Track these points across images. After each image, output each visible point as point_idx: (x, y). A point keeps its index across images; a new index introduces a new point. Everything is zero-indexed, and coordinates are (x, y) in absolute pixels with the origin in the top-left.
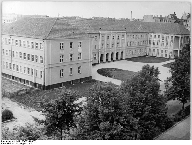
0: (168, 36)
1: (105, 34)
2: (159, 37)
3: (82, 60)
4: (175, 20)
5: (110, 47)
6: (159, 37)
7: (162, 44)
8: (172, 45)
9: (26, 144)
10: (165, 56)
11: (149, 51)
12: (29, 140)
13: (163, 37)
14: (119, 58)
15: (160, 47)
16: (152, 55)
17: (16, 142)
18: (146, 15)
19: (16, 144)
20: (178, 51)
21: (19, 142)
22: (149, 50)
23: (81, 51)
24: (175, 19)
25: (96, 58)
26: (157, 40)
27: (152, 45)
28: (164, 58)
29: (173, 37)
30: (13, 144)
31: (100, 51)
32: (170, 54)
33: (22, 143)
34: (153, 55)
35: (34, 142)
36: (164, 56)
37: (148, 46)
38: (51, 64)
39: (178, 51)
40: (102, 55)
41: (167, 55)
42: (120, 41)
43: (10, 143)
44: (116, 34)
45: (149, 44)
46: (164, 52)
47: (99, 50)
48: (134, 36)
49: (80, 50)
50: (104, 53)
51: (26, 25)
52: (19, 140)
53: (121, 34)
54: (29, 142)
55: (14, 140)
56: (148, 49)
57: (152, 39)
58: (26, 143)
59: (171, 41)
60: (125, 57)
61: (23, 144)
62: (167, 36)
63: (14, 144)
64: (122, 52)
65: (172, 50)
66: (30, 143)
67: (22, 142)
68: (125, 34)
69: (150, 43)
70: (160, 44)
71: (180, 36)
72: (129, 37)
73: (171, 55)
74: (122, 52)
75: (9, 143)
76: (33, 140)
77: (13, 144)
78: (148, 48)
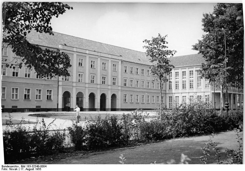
0: (185, 72)
2: (184, 73)
6: (184, 73)
7: (191, 86)
9: (33, 170)
11: (170, 101)
12: (37, 165)
15: (195, 90)
17: (21, 168)
19: (20, 169)
21: (24, 168)
22: (170, 99)
25: (52, 98)
27: (174, 90)
31: (60, 83)
33: (28, 168)
35: (44, 167)
37: (167, 92)
43: (13, 168)
44: (99, 59)
45: (169, 89)
47: (58, 81)
48: (139, 70)
50: (85, 92)
52: (24, 165)
54: (37, 167)
55: (18, 165)
56: (168, 98)
58: (33, 168)
60: (120, 106)
61: (30, 169)
63: (18, 169)
64: (114, 96)
67: (28, 167)
68: (118, 62)
70: (188, 85)
75: (12, 168)
76: (42, 165)
78: (168, 96)
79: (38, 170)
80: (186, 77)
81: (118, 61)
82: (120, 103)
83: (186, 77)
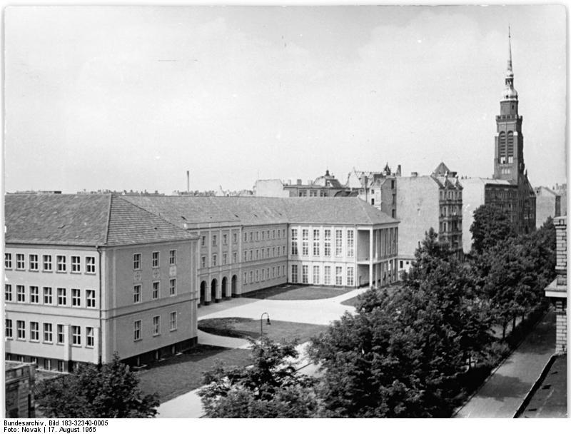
0: (341, 231)
1: (197, 231)
2: (327, 233)
3: (179, 296)
4: (335, 191)
5: (208, 265)
7: (327, 252)
8: (352, 252)
9: (77, 433)
10: (337, 280)
11: (293, 272)
12: (85, 420)
13: (327, 233)
14: (229, 294)
15: (332, 259)
16: (302, 282)
18: (260, 181)
20: (368, 266)
22: (293, 269)
23: (175, 273)
24: (338, 188)
26: (310, 241)
28: (335, 286)
29: (352, 231)
30: (37, 430)
32: (348, 275)
33: (65, 427)
34: (304, 282)
36: (333, 282)
37: (290, 258)
38: (117, 309)
39: (368, 266)
40: (203, 285)
41: (341, 277)
42: (208, 251)
43: (30, 427)
45: (293, 253)
46: (333, 270)
49: (173, 271)
51: (22, 215)
53: (230, 229)
54: (86, 426)
55: (41, 420)
56: (291, 267)
57: (299, 241)
58: (77, 427)
59: (350, 242)
60: (302, 280)
62: (337, 231)
63: (42, 430)
64: (234, 278)
65: (355, 266)
66: (89, 426)
67: (66, 422)
69: (295, 252)
71: (371, 229)
72: (249, 237)
73: (352, 278)
74: (234, 278)
75: (27, 427)
77: (37, 430)
78: (290, 264)
79: (89, 433)
80: (319, 238)
81: (218, 229)
82: (240, 287)
83: (319, 238)
